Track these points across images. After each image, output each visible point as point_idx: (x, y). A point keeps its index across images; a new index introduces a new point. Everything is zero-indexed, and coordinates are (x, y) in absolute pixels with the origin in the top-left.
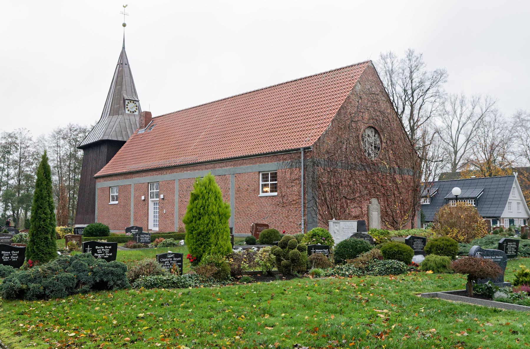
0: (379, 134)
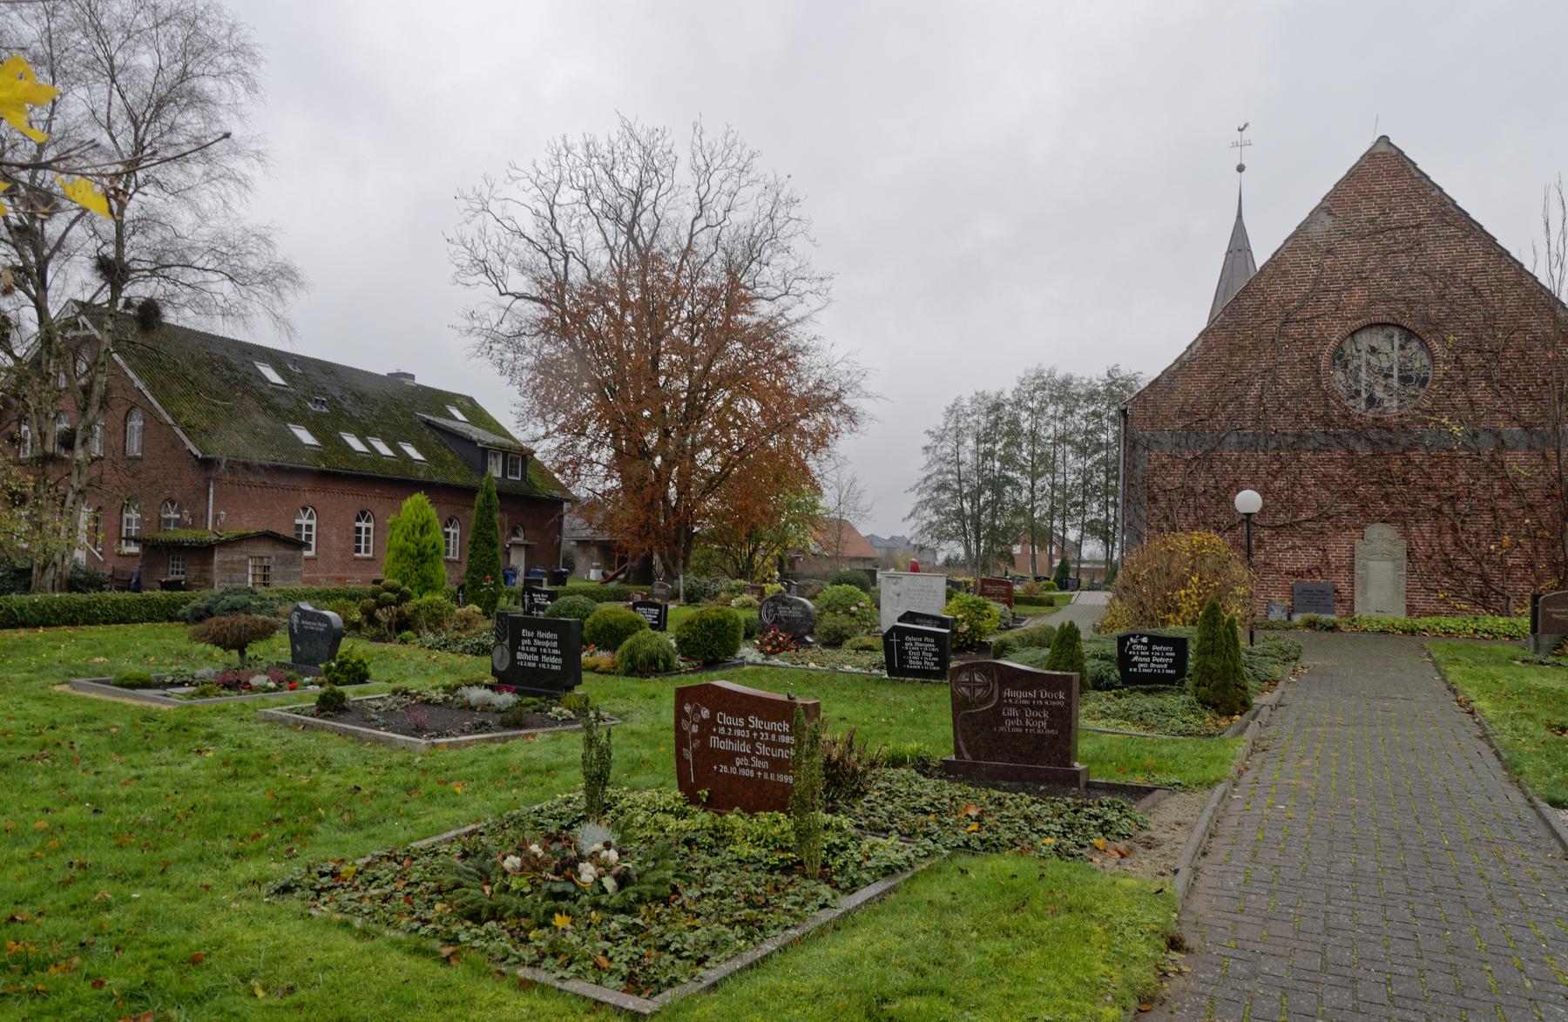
0: (1422, 340)
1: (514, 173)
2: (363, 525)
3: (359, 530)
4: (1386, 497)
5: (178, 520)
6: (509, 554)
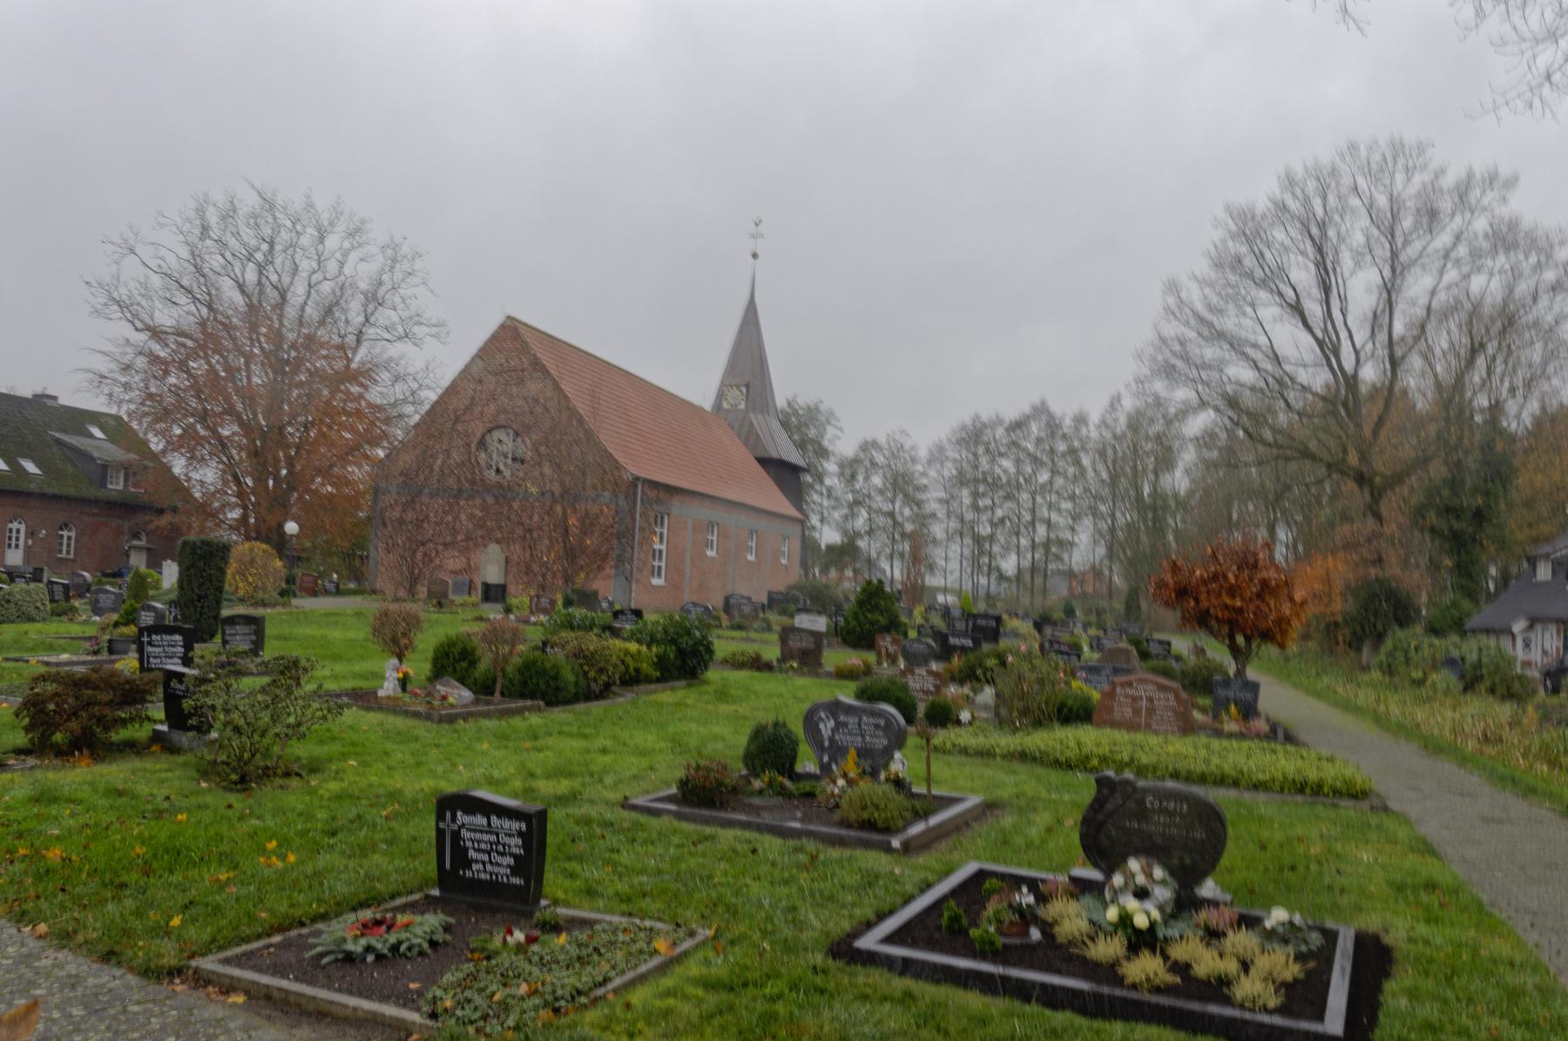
1: (163, 220)
2: (65, 533)
3: (62, 536)
4: (500, 528)
6: (128, 556)
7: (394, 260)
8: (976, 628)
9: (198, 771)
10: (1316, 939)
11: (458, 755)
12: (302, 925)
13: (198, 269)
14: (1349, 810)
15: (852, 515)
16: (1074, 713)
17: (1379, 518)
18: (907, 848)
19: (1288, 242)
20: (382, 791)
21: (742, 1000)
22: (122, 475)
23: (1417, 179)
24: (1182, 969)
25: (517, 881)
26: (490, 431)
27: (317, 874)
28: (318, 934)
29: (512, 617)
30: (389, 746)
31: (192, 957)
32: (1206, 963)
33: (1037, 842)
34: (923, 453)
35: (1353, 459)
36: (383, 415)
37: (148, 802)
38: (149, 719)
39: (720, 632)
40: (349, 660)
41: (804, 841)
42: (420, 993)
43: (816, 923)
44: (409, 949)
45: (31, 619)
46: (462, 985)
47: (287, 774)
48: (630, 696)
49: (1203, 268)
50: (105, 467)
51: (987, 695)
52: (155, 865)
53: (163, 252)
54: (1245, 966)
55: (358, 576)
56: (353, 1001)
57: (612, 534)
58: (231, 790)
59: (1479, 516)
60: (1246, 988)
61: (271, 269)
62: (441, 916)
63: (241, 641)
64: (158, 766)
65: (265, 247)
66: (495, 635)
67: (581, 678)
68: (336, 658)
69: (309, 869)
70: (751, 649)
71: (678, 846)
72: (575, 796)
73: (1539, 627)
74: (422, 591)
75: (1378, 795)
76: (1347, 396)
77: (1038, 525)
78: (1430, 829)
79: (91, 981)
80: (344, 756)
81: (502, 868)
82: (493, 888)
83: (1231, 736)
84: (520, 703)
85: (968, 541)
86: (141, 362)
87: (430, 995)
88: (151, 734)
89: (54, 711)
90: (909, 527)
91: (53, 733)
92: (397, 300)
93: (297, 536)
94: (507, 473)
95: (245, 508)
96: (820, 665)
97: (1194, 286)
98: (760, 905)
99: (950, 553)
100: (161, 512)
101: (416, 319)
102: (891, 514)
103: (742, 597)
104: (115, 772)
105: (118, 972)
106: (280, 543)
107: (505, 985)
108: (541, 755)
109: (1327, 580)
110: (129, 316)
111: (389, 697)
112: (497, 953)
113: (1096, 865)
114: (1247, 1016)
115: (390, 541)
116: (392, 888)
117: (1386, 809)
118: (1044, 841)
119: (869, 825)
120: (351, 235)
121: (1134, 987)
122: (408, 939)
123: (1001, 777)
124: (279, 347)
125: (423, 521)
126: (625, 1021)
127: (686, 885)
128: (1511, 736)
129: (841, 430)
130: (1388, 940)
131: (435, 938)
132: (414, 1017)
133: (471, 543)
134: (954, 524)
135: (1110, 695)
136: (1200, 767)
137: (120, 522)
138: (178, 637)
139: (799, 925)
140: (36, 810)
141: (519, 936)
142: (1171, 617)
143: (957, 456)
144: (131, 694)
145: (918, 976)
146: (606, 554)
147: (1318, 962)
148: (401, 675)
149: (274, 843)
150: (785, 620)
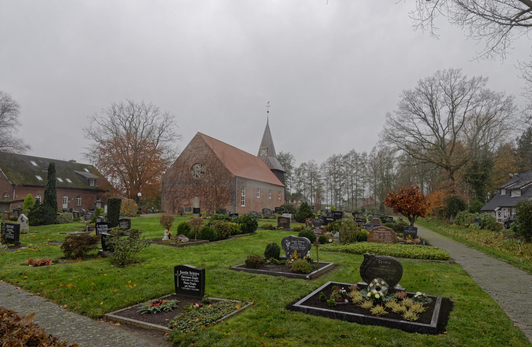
1: (103, 111)
2: (79, 199)
5: (7, 197)
6: (96, 204)
7: (167, 118)
8: (335, 215)
9: (111, 262)
10: (430, 300)
11: (184, 256)
12: (137, 304)
13: (113, 123)
14: (443, 263)
15: (300, 185)
16: (362, 238)
17: (453, 179)
18: (311, 278)
19: (421, 100)
20: (161, 266)
21: (260, 321)
22: (94, 181)
23: (459, 80)
24: (389, 310)
25: (197, 290)
26: (194, 165)
27: (142, 290)
28: (141, 306)
29: (201, 217)
30: (164, 254)
31: (106, 313)
32: (396, 308)
33: (349, 275)
34: (319, 166)
35: (444, 163)
36: (165, 162)
37: (96, 271)
38: (97, 248)
39: (260, 219)
40: (155, 231)
41: (281, 277)
42: (168, 321)
43: (283, 300)
44: (166, 309)
45: (68, 222)
46: (180, 319)
47: (135, 263)
48: (234, 238)
49: (397, 108)
50: (89, 180)
51: (337, 234)
52: (97, 288)
53: (103, 119)
54: (408, 308)
55: (159, 208)
56: (149, 324)
57: (229, 192)
58: (120, 267)
59: (483, 177)
60: (408, 314)
61: (133, 122)
62: (176, 300)
63: (124, 225)
64: (100, 261)
65: (131, 116)
66: (195, 222)
67: (219, 233)
68: (151, 230)
69: (140, 288)
70: (269, 223)
71: (244, 279)
72: (216, 266)
73: (503, 209)
74: (176, 211)
75: (452, 259)
76: (441, 144)
77: (353, 185)
78: (467, 268)
79: (78, 320)
80: (152, 257)
81: (193, 286)
82: (191, 292)
83: (409, 243)
84: (202, 241)
85: (333, 191)
86: (98, 150)
87: (171, 322)
88: (98, 252)
89: (71, 247)
90: (316, 188)
91: (71, 253)
92: (168, 129)
93: (141, 197)
94: (199, 176)
95: (128, 190)
96: (289, 228)
97: (394, 114)
98: (267, 295)
99: (328, 195)
100: (104, 192)
101: (173, 134)
102: (310, 184)
103: (268, 209)
104: (88, 263)
105: (85, 318)
106: (137, 199)
107: (192, 319)
108: (207, 255)
109: (439, 198)
110: (94, 137)
111: (165, 240)
112: (191, 310)
113: (365, 282)
114: (408, 322)
115: (167, 197)
116: (162, 293)
117: (454, 263)
118: (351, 275)
119: (300, 272)
120: (155, 112)
121: (375, 315)
122: (166, 307)
123: (340, 257)
124: (136, 144)
125: (176, 191)
126: (226, 328)
127: (246, 290)
128: (495, 241)
129: (295, 160)
130: (452, 300)
131: (174, 306)
132: (167, 328)
133: (189, 197)
134: (329, 186)
135: (372, 233)
136: (398, 253)
137: (93, 195)
138: (106, 225)
139: (278, 300)
140: (65, 274)
141: (197, 305)
142: (391, 210)
143: (329, 166)
144: (92, 241)
145: (312, 314)
146: (228, 199)
147: (430, 307)
148: (168, 234)
149: (130, 281)
150: (280, 215)
